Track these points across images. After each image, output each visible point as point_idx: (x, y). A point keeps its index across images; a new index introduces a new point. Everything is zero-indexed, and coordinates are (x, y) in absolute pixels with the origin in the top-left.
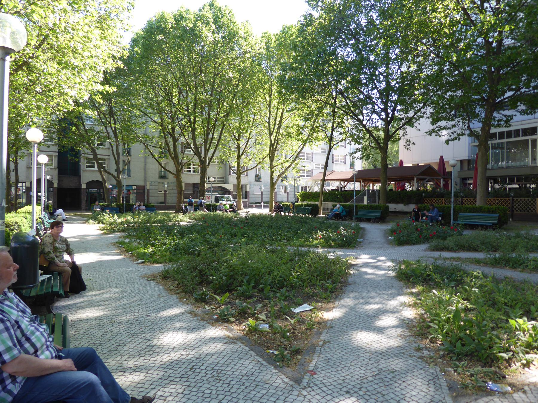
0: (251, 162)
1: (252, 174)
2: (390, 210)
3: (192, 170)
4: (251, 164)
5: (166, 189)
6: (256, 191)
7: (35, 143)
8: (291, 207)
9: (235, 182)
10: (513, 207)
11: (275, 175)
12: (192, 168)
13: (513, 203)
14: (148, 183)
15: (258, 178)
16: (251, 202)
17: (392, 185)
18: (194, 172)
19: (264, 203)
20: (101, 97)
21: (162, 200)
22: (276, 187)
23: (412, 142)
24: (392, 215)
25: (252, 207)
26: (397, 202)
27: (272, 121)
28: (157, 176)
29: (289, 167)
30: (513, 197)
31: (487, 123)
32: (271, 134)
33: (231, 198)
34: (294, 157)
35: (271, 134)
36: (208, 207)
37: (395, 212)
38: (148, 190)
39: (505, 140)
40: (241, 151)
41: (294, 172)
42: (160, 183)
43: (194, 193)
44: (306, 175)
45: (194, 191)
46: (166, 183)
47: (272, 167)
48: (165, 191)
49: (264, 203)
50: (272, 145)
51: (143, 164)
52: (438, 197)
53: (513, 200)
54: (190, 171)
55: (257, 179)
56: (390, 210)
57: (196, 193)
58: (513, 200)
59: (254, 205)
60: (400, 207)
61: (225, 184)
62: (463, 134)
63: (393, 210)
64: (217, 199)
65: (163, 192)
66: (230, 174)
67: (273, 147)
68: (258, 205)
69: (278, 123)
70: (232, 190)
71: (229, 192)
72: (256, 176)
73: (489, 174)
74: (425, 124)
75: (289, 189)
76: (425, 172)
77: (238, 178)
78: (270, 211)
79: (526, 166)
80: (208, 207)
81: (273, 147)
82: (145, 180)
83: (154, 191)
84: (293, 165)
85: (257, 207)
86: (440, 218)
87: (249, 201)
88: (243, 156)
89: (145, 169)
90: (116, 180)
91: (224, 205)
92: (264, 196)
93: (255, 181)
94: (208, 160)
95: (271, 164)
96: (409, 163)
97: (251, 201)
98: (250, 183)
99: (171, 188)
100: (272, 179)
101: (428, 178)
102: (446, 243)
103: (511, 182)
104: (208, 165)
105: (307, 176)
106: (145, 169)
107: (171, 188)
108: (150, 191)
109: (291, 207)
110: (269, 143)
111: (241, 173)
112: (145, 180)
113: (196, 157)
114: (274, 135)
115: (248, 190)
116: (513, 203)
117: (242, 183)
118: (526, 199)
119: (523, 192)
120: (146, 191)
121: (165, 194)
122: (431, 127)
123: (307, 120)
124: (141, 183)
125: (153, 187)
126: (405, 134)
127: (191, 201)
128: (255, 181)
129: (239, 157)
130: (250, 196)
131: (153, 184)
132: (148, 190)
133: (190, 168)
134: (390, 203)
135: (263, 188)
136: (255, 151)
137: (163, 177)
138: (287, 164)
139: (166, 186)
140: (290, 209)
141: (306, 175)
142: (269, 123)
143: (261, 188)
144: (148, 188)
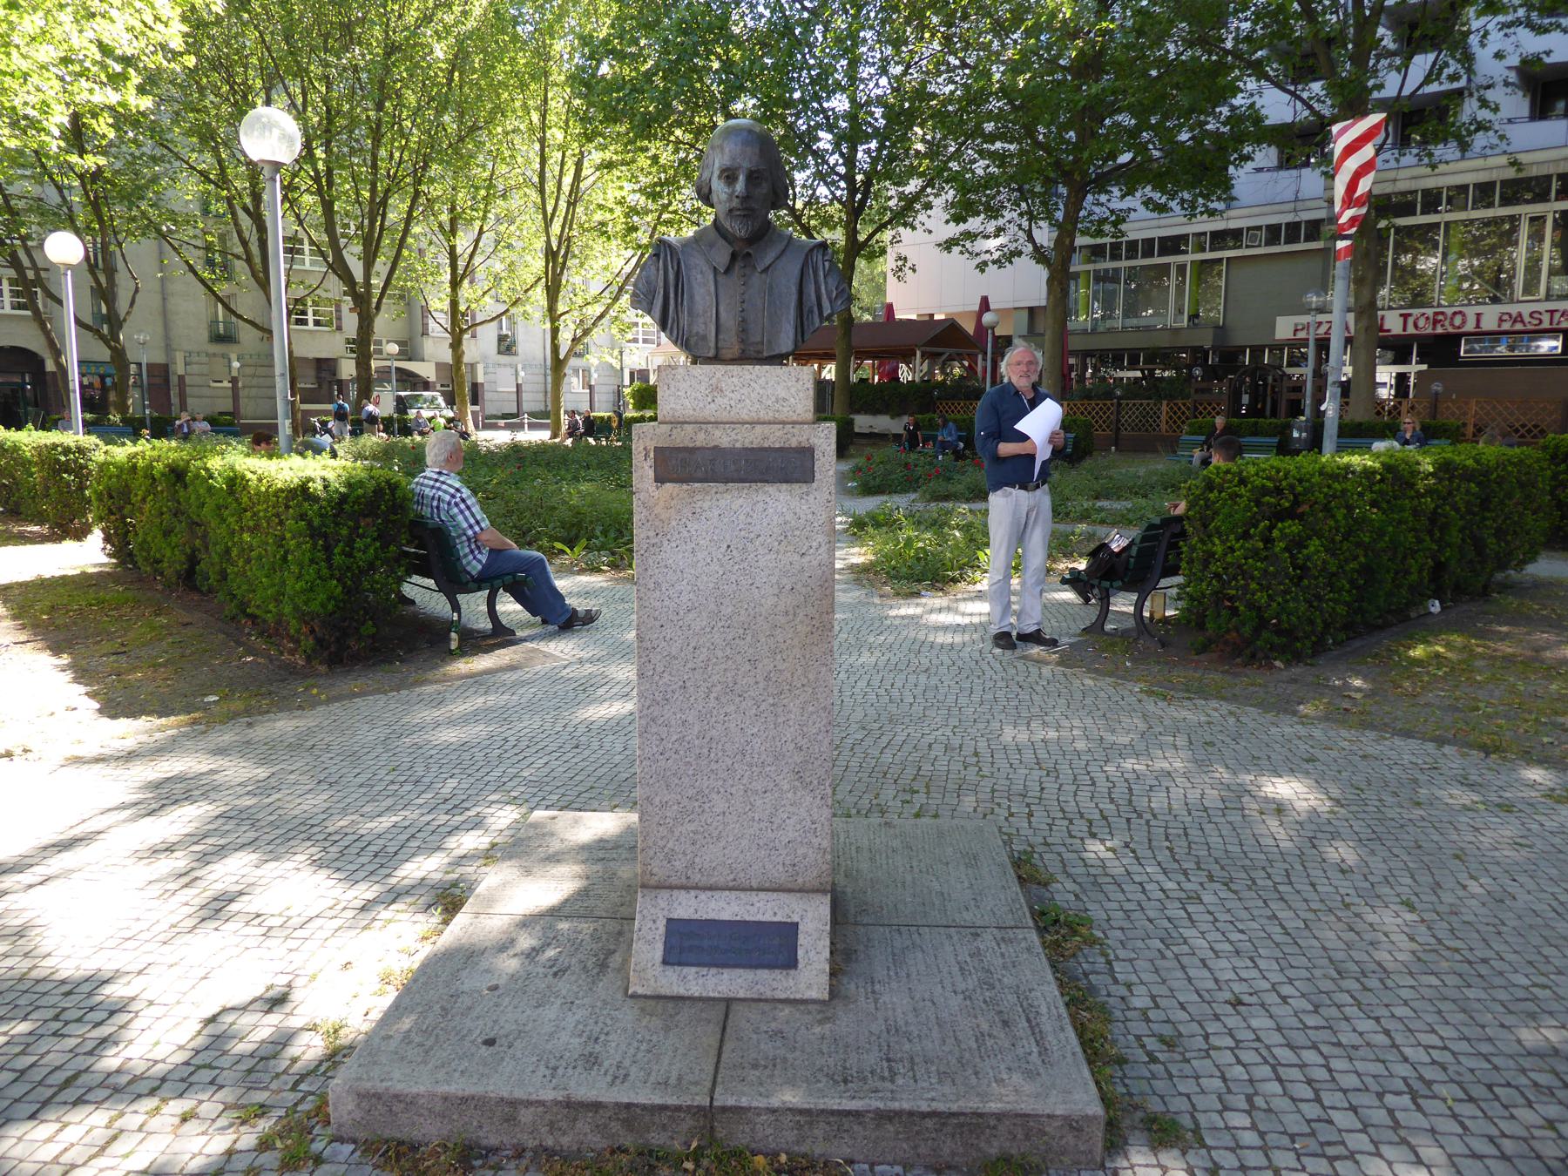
0: (487, 298)
1: (488, 335)
2: (857, 430)
3: (310, 318)
4: (489, 306)
5: (234, 374)
6: (498, 381)
7: (68, 266)
8: (614, 425)
9: (447, 356)
10: (1118, 421)
11: (565, 337)
12: (310, 312)
13: (1119, 413)
14: (179, 358)
15: (506, 346)
16: (488, 412)
17: (868, 371)
18: (317, 323)
19: (532, 415)
20: (111, 121)
21: (227, 405)
22: (567, 370)
23: (909, 264)
24: (864, 441)
25: (494, 427)
26: (875, 411)
27: (550, 186)
28: (205, 335)
29: (602, 316)
30: (1119, 398)
31: (1066, 231)
32: (548, 222)
33: (441, 401)
34: (615, 288)
35: (548, 222)
36: (388, 425)
37: (871, 436)
38: (181, 378)
39: (1124, 264)
40: (461, 264)
41: (615, 331)
42: (214, 355)
43: (320, 386)
44: (640, 337)
45: (319, 380)
46: (233, 356)
47: (553, 314)
48: (234, 381)
49: (532, 415)
50: (550, 254)
51: (158, 298)
52: (969, 399)
53: (1119, 405)
54: (305, 322)
55: (503, 348)
56: (857, 430)
57: (325, 386)
58: (1119, 405)
59: (502, 422)
60: (883, 423)
61: (410, 360)
62: (1020, 253)
63: (867, 431)
64: (402, 405)
65: (226, 384)
66: (425, 333)
67: (557, 260)
68: (512, 420)
69: (566, 188)
70: (432, 378)
71: (427, 386)
72: (502, 339)
73: (1075, 343)
74: (936, 221)
75: (595, 376)
76: (943, 338)
77: (456, 345)
78: (554, 436)
79: (1149, 329)
80: (388, 425)
81: (557, 260)
82: (169, 348)
83: (198, 380)
84: (612, 313)
85: (508, 427)
86: (962, 445)
87: (483, 409)
88: (466, 283)
89: (164, 313)
90: (110, 347)
91: (430, 419)
92: (525, 396)
93: (499, 353)
94: (376, 292)
95: (552, 308)
96: (910, 310)
97: (490, 410)
98: (485, 358)
99: (248, 371)
100: (555, 349)
101: (948, 351)
102: (952, 488)
103: (1117, 361)
104: (378, 308)
105: (645, 341)
106: (164, 313)
107: (248, 371)
108: (188, 380)
109: (614, 425)
110: (540, 244)
111: (463, 331)
112: (169, 348)
113: (333, 278)
114: (556, 228)
115: (480, 379)
116: (1119, 413)
117: (466, 359)
118: (1145, 402)
119: (1152, 389)
120: (174, 380)
121: (235, 389)
122: (954, 230)
123: (654, 196)
124: (159, 358)
125: (195, 369)
126: (895, 240)
127: (341, 407)
128: (499, 353)
129: (455, 284)
130: (487, 396)
131: (195, 359)
132: (181, 378)
133: (304, 313)
134: (858, 412)
135: (522, 374)
136: (498, 267)
137: (223, 338)
138: (597, 309)
139: (236, 364)
140: (610, 429)
141: (640, 337)
142: (542, 191)
143: (517, 374)
144: (181, 371)
